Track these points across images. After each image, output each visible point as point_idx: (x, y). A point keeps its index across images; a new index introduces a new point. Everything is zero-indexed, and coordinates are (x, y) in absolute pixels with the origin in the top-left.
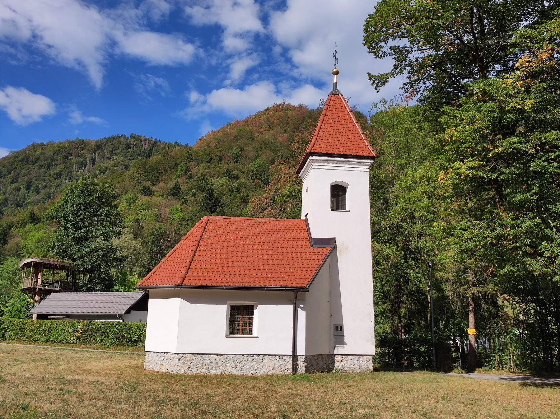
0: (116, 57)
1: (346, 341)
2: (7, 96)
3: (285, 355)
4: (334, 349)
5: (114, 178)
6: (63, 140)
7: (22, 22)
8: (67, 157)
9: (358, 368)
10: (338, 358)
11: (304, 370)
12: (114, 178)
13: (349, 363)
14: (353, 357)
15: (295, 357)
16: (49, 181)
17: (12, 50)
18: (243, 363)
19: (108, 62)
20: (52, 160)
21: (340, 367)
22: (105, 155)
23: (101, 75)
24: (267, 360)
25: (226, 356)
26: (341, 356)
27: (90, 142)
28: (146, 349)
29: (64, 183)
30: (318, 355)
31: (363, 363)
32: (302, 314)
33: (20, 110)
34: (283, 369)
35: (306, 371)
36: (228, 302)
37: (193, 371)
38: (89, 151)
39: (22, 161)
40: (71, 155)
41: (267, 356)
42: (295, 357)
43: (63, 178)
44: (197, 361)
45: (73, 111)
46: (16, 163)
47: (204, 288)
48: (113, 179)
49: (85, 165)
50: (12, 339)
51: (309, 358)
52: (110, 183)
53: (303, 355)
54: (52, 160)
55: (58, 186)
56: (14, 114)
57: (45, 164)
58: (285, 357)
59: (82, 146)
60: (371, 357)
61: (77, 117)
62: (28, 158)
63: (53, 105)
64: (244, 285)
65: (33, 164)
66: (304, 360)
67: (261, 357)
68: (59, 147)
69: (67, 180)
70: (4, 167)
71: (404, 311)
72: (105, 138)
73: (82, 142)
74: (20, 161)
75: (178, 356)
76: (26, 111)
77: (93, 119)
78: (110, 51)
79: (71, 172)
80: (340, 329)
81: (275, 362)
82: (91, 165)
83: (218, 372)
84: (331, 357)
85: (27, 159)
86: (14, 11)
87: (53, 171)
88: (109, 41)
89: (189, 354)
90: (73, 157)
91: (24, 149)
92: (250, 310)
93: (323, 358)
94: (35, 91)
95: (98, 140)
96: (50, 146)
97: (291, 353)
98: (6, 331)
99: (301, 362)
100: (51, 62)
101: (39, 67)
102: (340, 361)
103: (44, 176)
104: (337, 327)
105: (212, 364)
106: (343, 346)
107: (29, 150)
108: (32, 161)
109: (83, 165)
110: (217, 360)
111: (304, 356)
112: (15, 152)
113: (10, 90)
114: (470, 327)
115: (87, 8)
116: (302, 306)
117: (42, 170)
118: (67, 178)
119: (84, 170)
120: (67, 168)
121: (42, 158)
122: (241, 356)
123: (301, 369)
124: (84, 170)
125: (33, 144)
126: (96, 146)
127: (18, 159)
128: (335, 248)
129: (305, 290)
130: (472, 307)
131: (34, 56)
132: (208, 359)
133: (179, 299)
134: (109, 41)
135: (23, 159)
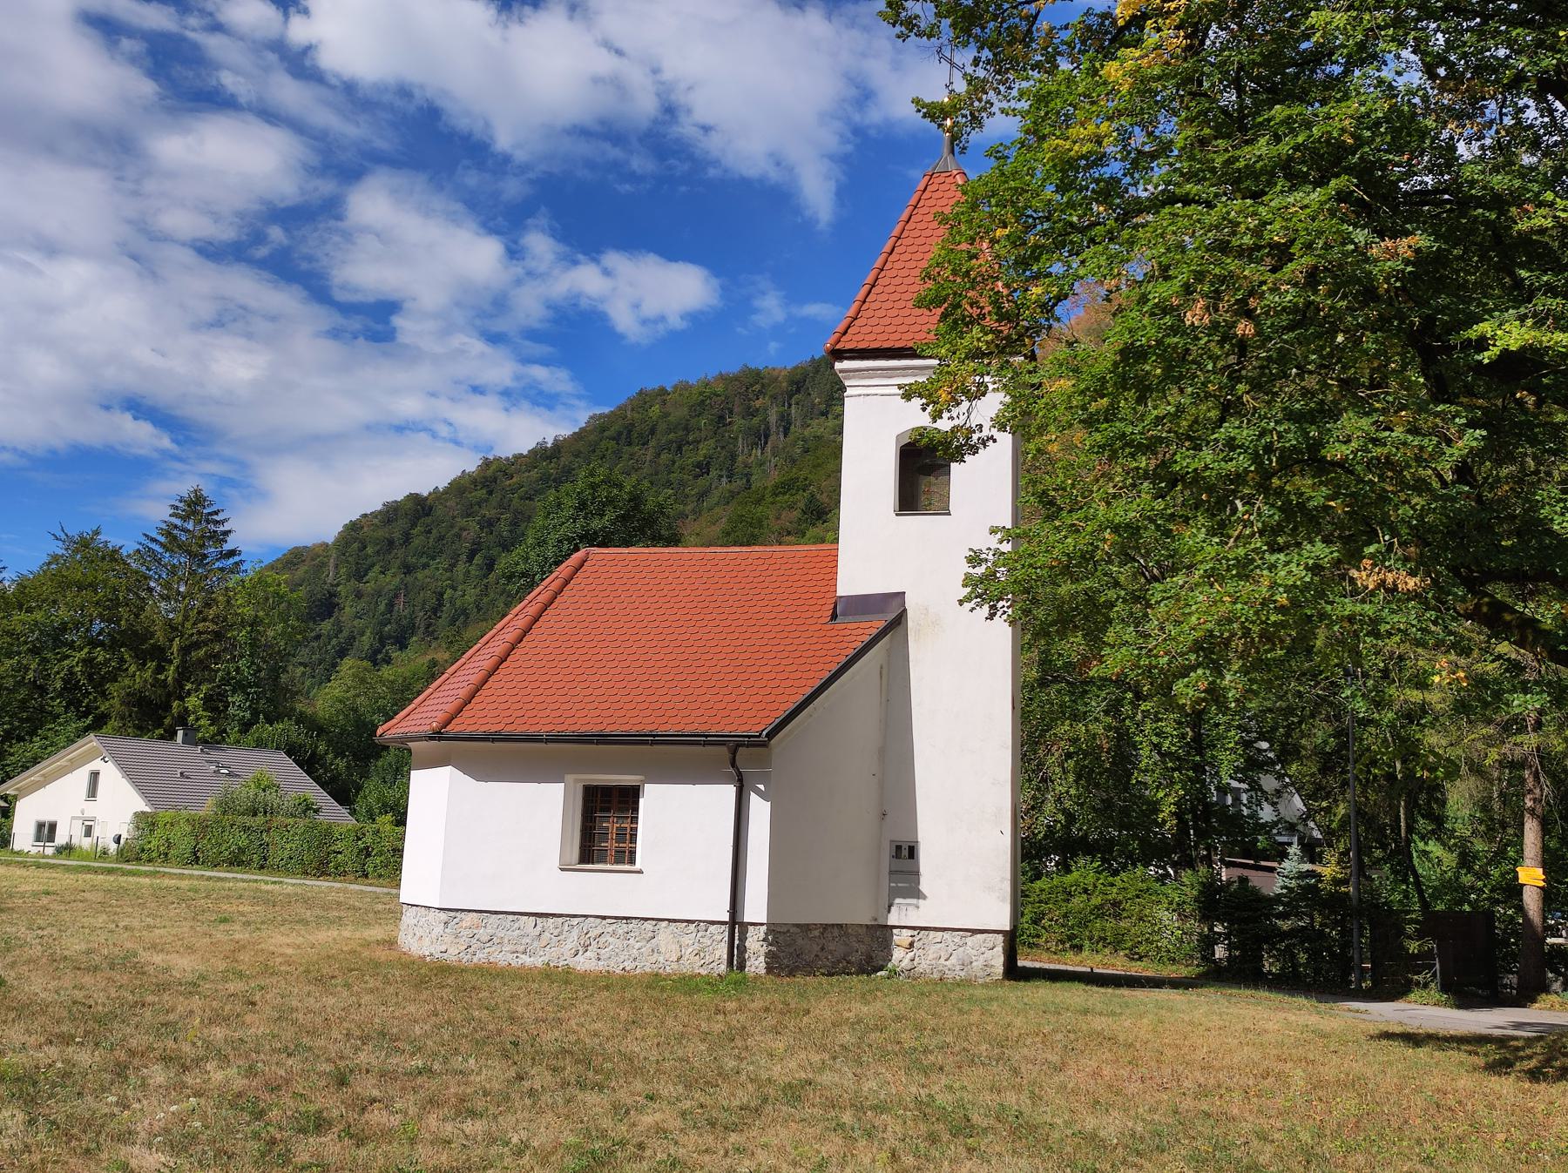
0: (872, 132)
1: (923, 887)
2: (607, 273)
3: (713, 923)
4: (889, 911)
5: (819, 465)
6: (711, 373)
7: (637, 77)
8: (721, 418)
9: (958, 968)
10: (901, 937)
11: (764, 965)
12: (819, 465)
13: (932, 952)
14: (947, 935)
15: (736, 923)
16: (682, 484)
17: (615, 153)
18: (602, 940)
19: (849, 148)
20: (687, 429)
21: (906, 964)
22: (813, 405)
23: (831, 186)
24: (665, 934)
25: (560, 920)
26: (910, 932)
27: (775, 373)
28: (405, 896)
29: (716, 488)
30: (826, 927)
31: (974, 952)
32: (760, 811)
33: (636, 306)
34: (708, 959)
35: (769, 969)
36: (570, 778)
37: (480, 955)
38: (774, 397)
39: (617, 438)
40: (731, 412)
41: (665, 924)
42: (736, 923)
43: (713, 473)
44: (490, 931)
45: (763, 293)
46: (603, 444)
47: (494, 740)
48: (814, 467)
49: (767, 437)
50: (380, 876)
51: (775, 932)
52: (806, 479)
53: (762, 924)
54: (687, 429)
55: (703, 495)
56: (623, 319)
57: (671, 442)
58: (712, 928)
59: (757, 387)
60: (1000, 938)
61: (771, 307)
62: (630, 428)
63: (715, 282)
64: (596, 729)
65: (644, 444)
66: (762, 936)
67: (649, 925)
68: (701, 393)
69: (724, 480)
70: (577, 456)
71: (1343, 812)
72: (813, 359)
73: (757, 376)
74: (613, 439)
75: (443, 916)
76: (651, 308)
77: (813, 310)
78: (857, 118)
79: (733, 457)
80: (907, 853)
81: (687, 940)
82: (782, 436)
83: (538, 961)
84: (881, 934)
85: (630, 432)
86: (619, 53)
87: (692, 457)
88: (853, 92)
89: (470, 911)
90: (736, 418)
91: (620, 408)
92: (627, 799)
93: (847, 935)
94: (672, 252)
95: (796, 368)
96: (680, 395)
97: (726, 918)
98: (368, 855)
99: (756, 944)
100: (712, 172)
101: (683, 189)
102: (906, 944)
103: (669, 473)
104: (899, 848)
105: (524, 941)
106: (914, 901)
107: (633, 410)
108: (641, 435)
109: (760, 437)
110: (539, 928)
111: (765, 927)
112: (602, 416)
113: (612, 259)
114: (1528, 862)
115: (795, 10)
116: (761, 787)
117: (665, 457)
118: (724, 473)
119: (763, 449)
120: (723, 448)
121: (662, 427)
122: (599, 920)
123: (756, 964)
124: (763, 449)
125: (641, 393)
126: (792, 382)
127: (607, 434)
128: (899, 621)
129: (760, 743)
130: (1535, 800)
131: (672, 161)
132: (517, 925)
133: (449, 768)
134: (853, 92)
135: (620, 434)
